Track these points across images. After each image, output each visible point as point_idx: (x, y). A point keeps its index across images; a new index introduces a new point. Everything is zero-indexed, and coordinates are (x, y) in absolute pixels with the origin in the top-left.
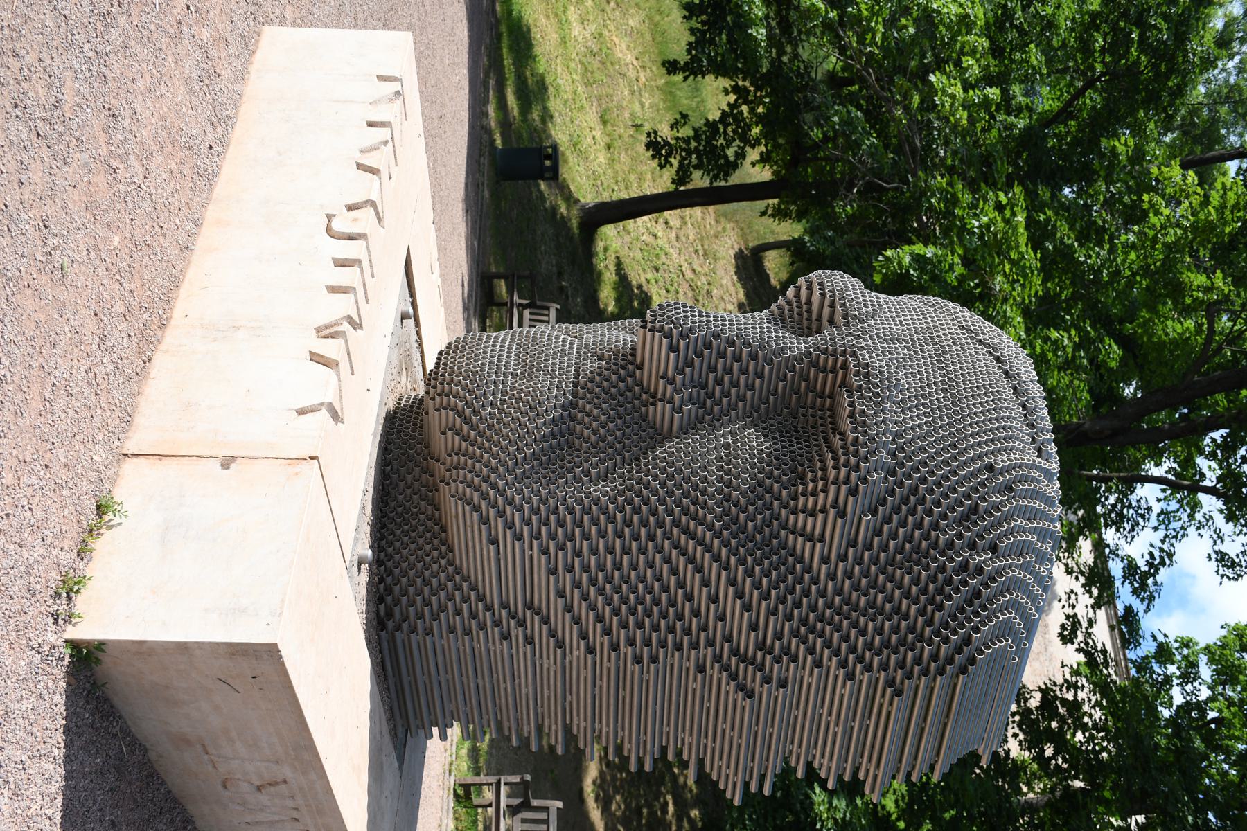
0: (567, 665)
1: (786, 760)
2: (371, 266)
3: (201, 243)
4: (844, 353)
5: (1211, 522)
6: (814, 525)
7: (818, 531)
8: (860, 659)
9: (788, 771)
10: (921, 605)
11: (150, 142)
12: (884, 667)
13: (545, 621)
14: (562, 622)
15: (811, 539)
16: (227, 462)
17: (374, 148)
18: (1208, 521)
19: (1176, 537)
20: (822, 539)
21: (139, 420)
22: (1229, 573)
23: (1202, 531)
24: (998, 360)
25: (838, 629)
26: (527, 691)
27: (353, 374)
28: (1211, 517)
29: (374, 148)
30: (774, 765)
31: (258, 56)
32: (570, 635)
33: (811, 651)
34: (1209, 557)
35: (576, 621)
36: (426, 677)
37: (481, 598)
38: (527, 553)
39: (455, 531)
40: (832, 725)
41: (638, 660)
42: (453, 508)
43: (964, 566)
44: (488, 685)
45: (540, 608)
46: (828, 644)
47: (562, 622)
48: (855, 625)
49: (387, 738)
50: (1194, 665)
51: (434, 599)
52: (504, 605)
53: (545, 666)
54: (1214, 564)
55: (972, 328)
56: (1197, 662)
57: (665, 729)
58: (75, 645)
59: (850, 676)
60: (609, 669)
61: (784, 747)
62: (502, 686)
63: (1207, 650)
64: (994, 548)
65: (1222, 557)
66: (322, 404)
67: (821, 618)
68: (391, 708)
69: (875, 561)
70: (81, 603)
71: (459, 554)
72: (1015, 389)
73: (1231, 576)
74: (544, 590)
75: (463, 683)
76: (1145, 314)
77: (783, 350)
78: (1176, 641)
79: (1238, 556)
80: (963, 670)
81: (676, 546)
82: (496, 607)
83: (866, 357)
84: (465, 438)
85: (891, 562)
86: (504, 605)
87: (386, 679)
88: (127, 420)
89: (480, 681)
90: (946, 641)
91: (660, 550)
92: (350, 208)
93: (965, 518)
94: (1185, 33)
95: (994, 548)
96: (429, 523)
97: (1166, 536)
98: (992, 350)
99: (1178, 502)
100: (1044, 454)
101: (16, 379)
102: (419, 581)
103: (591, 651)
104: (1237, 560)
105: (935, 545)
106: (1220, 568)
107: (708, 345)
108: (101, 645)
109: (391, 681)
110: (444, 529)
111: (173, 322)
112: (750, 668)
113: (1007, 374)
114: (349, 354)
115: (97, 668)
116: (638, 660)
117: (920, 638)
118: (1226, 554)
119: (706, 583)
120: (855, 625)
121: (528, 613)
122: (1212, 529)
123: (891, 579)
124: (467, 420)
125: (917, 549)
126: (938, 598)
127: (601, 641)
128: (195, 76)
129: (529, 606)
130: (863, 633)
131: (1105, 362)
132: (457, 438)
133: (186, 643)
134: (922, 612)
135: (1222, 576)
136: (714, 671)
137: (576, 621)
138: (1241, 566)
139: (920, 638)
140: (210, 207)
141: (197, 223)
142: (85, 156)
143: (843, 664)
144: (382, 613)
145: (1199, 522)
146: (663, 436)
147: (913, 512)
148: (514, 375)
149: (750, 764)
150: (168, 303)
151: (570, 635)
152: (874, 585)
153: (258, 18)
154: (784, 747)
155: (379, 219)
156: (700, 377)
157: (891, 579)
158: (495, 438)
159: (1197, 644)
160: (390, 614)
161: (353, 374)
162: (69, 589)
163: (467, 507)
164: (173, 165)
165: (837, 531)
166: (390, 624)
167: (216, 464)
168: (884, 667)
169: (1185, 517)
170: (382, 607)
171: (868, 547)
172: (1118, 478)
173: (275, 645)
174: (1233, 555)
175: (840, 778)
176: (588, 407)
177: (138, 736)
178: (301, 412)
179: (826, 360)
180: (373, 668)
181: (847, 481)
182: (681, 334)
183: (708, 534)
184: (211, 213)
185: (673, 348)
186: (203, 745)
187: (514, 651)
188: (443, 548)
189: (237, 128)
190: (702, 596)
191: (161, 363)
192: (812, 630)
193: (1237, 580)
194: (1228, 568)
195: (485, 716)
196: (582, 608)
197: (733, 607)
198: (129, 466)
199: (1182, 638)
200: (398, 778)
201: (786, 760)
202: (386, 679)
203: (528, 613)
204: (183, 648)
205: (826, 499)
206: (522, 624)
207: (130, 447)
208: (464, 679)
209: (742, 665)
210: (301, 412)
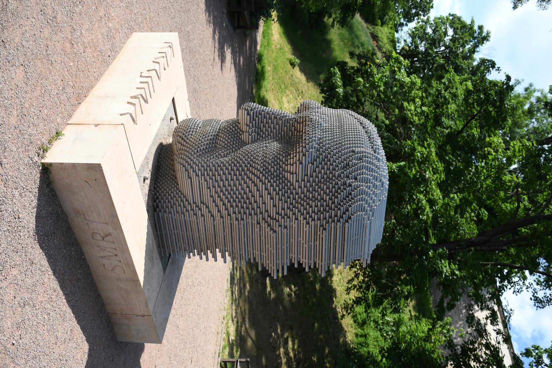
0: (215, 224)
1: (291, 260)
2: (153, 88)
3: (102, 79)
4: (306, 117)
5: (532, 286)
6: (293, 169)
7: (294, 171)
8: (311, 217)
9: (292, 265)
11: (87, 43)
12: (319, 219)
13: (207, 207)
14: (212, 206)
15: (292, 174)
16: (96, 125)
17: (159, 58)
18: (530, 285)
19: (518, 292)
20: (296, 173)
21: (73, 116)
22: (540, 305)
23: (528, 290)
24: (361, 123)
25: (303, 205)
26: (203, 236)
27: (142, 114)
28: (532, 284)
29: (159, 58)
30: (287, 263)
31: (130, 39)
32: (215, 212)
33: (294, 214)
34: (531, 299)
35: (217, 206)
36: (170, 231)
37: (187, 200)
38: (201, 182)
39: (179, 175)
40: (304, 244)
41: (237, 219)
42: (178, 167)
43: (345, 184)
44: (190, 235)
45: (206, 203)
46: (299, 211)
47: (212, 206)
48: (308, 204)
49: (156, 252)
50: (540, 357)
51: (172, 200)
53: (208, 225)
54: (533, 302)
56: (542, 356)
57: (249, 249)
58: (43, 164)
59: (308, 223)
60: (228, 224)
61: (290, 255)
62: (195, 235)
63: (546, 351)
64: (356, 179)
65: (537, 300)
66: (128, 113)
67: (297, 202)
68: (159, 243)
70: (47, 154)
71: (180, 186)
73: (541, 306)
74: (207, 198)
75: (182, 234)
77: (286, 116)
78: (532, 347)
79: (543, 298)
80: (347, 221)
81: (248, 177)
82: (192, 203)
85: (320, 182)
86: (194, 203)
87: (157, 231)
88: (70, 116)
89: (188, 233)
90: (340, 209)
91: (243, 179)
92: (148, 71)
93: (345, 167)
94: (503, 98)
95: (356, 179)
96: (172, 176)
97: (514, 291)
98: (359, 121)
99: (518, 277)
100: (376, 152)
101: (33, 81)
102: (167, 194)
103: (222, 217)
104: (542, 300)
106: (536, 304)
108: (51, 165)
109: (159, 233)
110: (176, 178)
111: (89, 96)
112: (274, 221)
113: (364, 128)
114: (141, 106)
115: (50, 175)
116: (237, 219)
117: (331, 209)
118: (538, 297)
119: (258, 190)
120: (308, 204)
121: (202, 204)
122: (533, 288)
123: (320, 187)
126: (336, 194)
127: (224, 213)
128: (106, 34)
129: (202, 202)
130: (311, 207)
131: (482, 218)
132: (180, 145)
133: (75, 164)
134: (330, 199)
135: (537, 307)
136: (263, 224)
137: (217, 206)
138: (544, 302)
139: (331, 209)
140: (107, 72)
141: (102, 74)
142: (63, 36)
143: (305, 218)
144: (155, 206)
145: (527, 286)
146: (244, 144)
149: (278, 262)
150: (88, 91)
151: (215, 212)
152: (314, 190)
153: (132, 30)
154: (290, 255)
156: (258, 125)
157: (320, 187)
158: (191, 144)
159: (542, 349)
160: (158, 207)
161: (142, 114)
162: (45, 151)
163: (181, 166)
164: (95, 54)
165: (300, 169)
166: (158, 209)
167: (94, 126)
168: (319, 219)
169: (521, 283)
170: (155, 203)
172: (491, 264)
173: (100, 164)
174: (541, 298)
175: (310, 268)
176: (222, 135)
177: (65, 210)
178: (121, 115)
179: (300, 120)
180: (149, 219)
181: (302, 151)
182: (251, 110)
183: (258, 172)
184: (107, 72)
186: (84, 215)
187: (198, 220)
188: (176, 184)
189: (119, 55)
190: (257, 194)
191: (83, 105)
192: (294, 207)
193: (543, 308)
194: (539, 303)
195: (190, 248)
196: (218, 200)
197: (267, 198)
198: (68, 126)
199: (535, 346)
200: (162, 273)
201: (291, 260)
202: (157, 231)
203: (202, 204)
204: (74, 166)
205: (296, 158)
206: (200, 209)
207: (69, 122)
208: (183, 232)
209: (271, 220)
210: (121, 115)
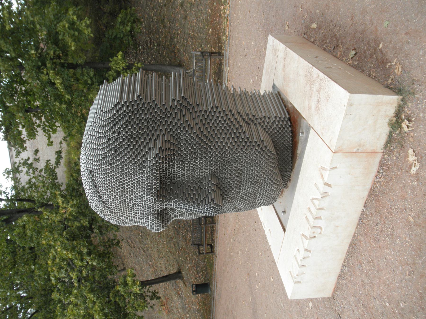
7: (167, 144)
10: (157, 107)
24: (104, 202)
52: (255, 124)
55: (111, 213)
69: (148, 135)
72: (98, 192)
76: (16, 245)
83: (151, 199)
84: (272, 171)
105: (129, 140)
107: (202, 202)
113: (101, 197)
114: (326, 145)
124: (272, 177)
125: (135, 139)
147: (137, 150)
148: (258, 192)
155: (290, 273)
171: (150, 139)
185: (213, 200)
